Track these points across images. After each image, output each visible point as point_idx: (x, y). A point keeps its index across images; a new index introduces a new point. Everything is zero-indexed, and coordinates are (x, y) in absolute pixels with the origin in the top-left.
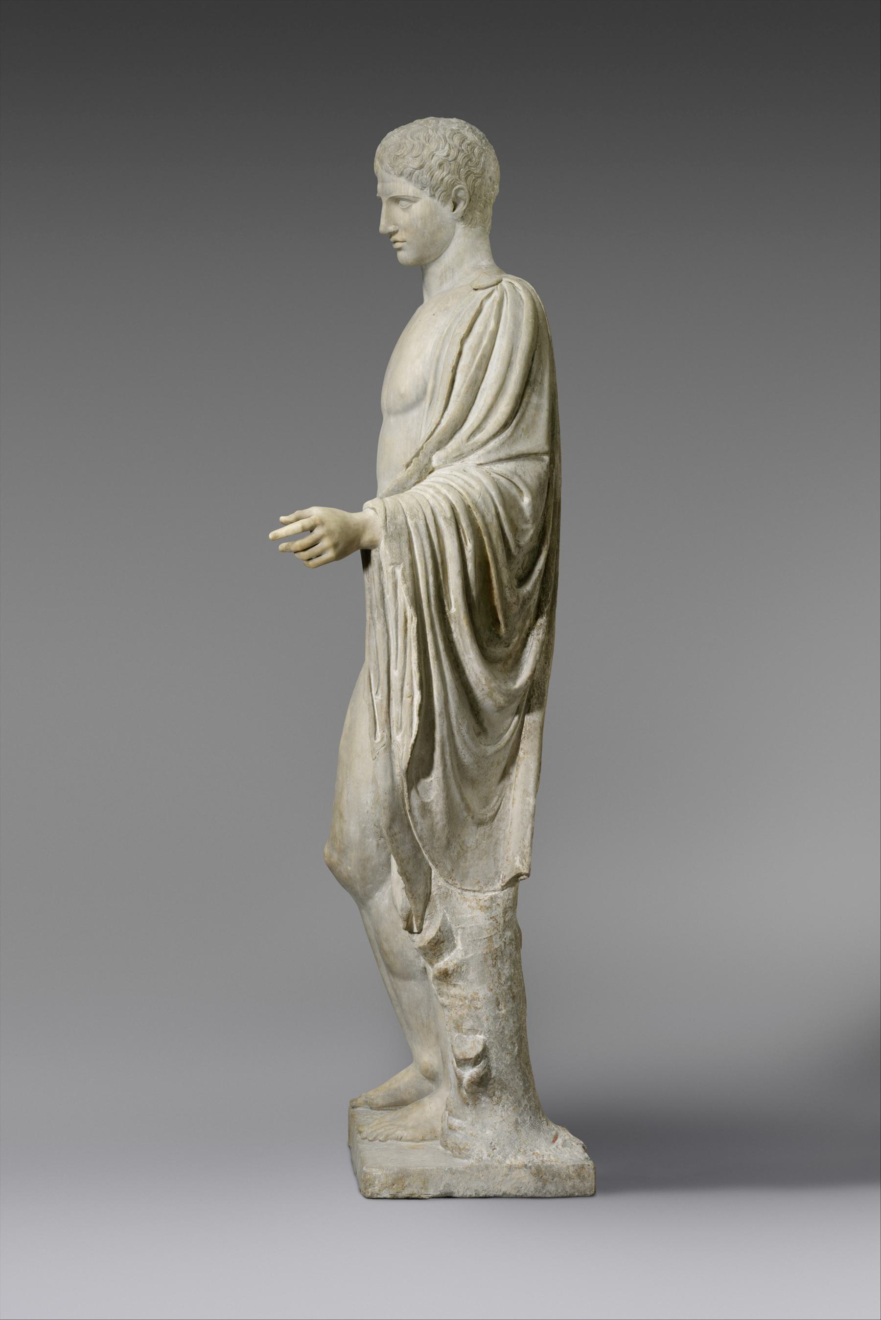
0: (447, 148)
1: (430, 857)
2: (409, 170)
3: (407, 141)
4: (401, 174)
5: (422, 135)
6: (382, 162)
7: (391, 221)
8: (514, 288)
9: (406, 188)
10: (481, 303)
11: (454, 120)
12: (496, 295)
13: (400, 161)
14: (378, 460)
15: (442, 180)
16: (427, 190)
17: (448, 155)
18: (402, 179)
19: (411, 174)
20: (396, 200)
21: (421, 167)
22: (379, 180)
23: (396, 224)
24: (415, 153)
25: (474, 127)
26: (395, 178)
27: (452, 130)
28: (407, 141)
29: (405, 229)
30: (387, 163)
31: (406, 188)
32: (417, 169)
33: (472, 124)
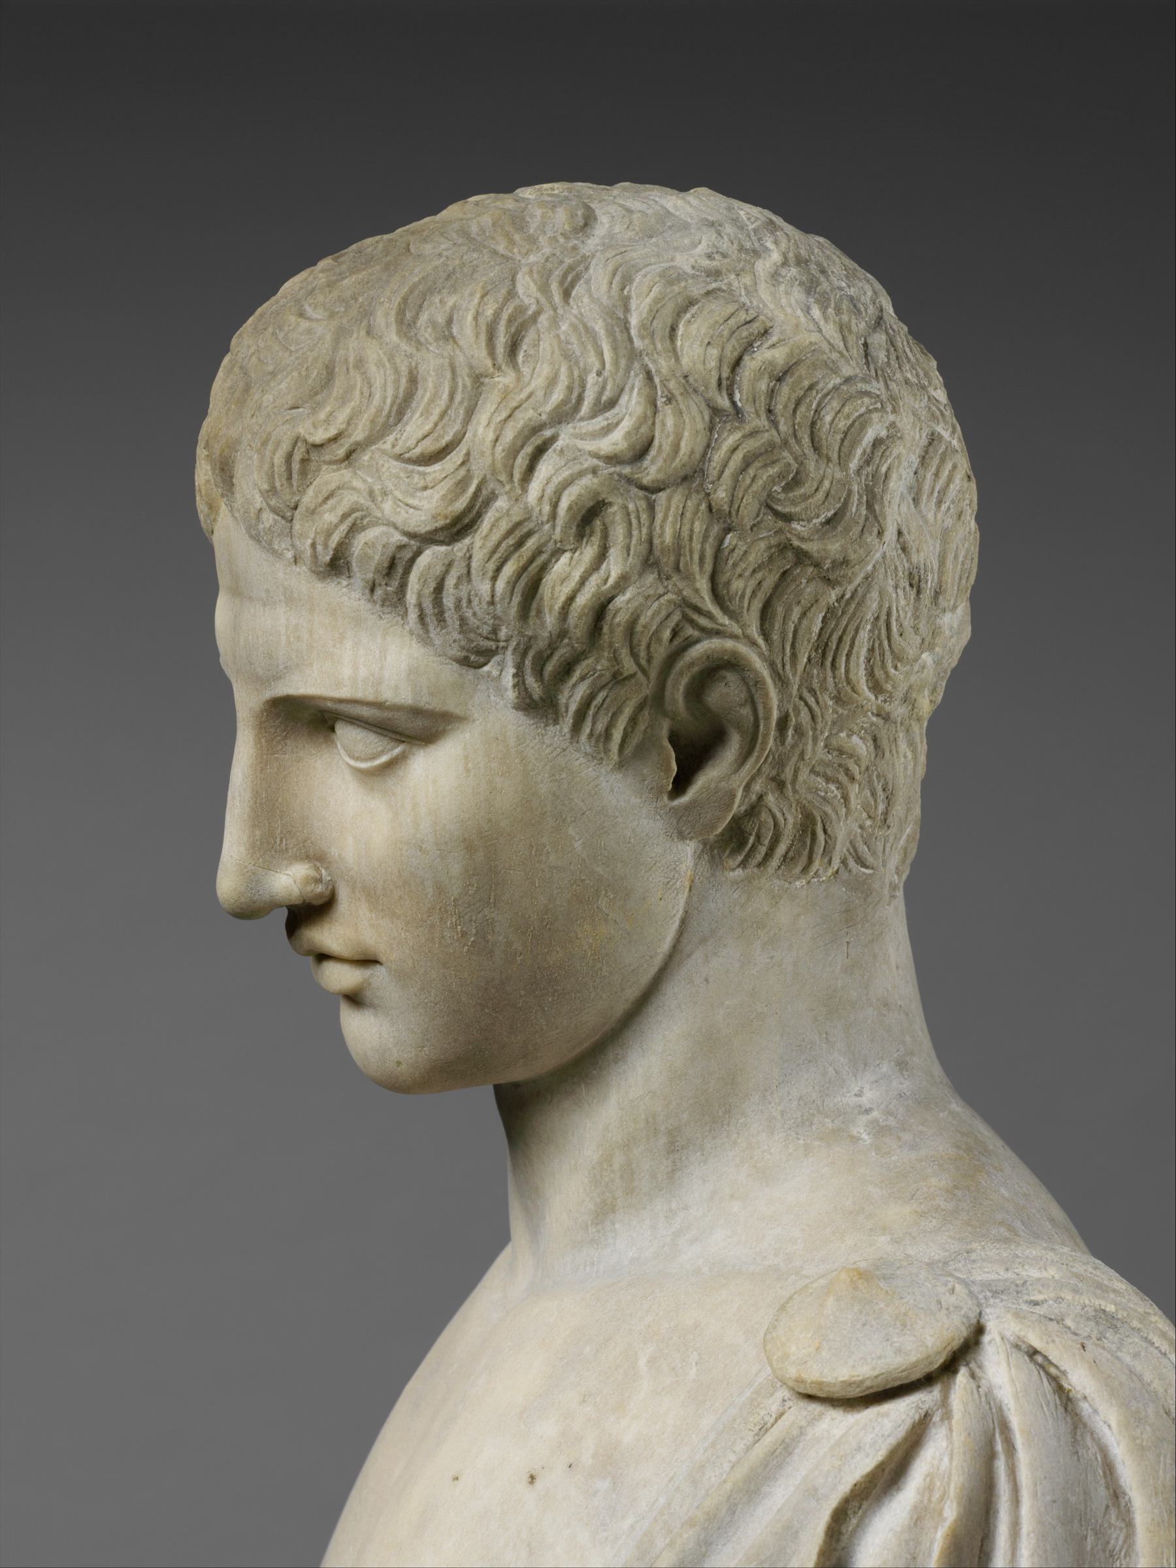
0: (632, 404)
1: (667, 261)
2: (374, 542)
3: (373, 353)
4: (337, 565)
5: (469, 308)
6: (225, 471)
7: (278, 834)
8: (1065, 1399)
9: (368, 656)
10: (840, 1516)
11: (697, 205)
12: (942, 1462)
13: (328, 477)
14: (354, 1493)
15: (600, 611)
16: (503, 672)
17: (641, 452)
18: (346, 596)
19: (395, 568)
20: (307, 719)
21: (459, 527)
22: (223, 579)
23: (318, 858)
24: (414, 432)
25: (818, 247)
26: (301, 580)
27: (671, 277)
28: (373, 353)
29: (371, 895)
30: (251, 483)
31: (368, 656)
32: (429, 539)
33: (806, 225)
